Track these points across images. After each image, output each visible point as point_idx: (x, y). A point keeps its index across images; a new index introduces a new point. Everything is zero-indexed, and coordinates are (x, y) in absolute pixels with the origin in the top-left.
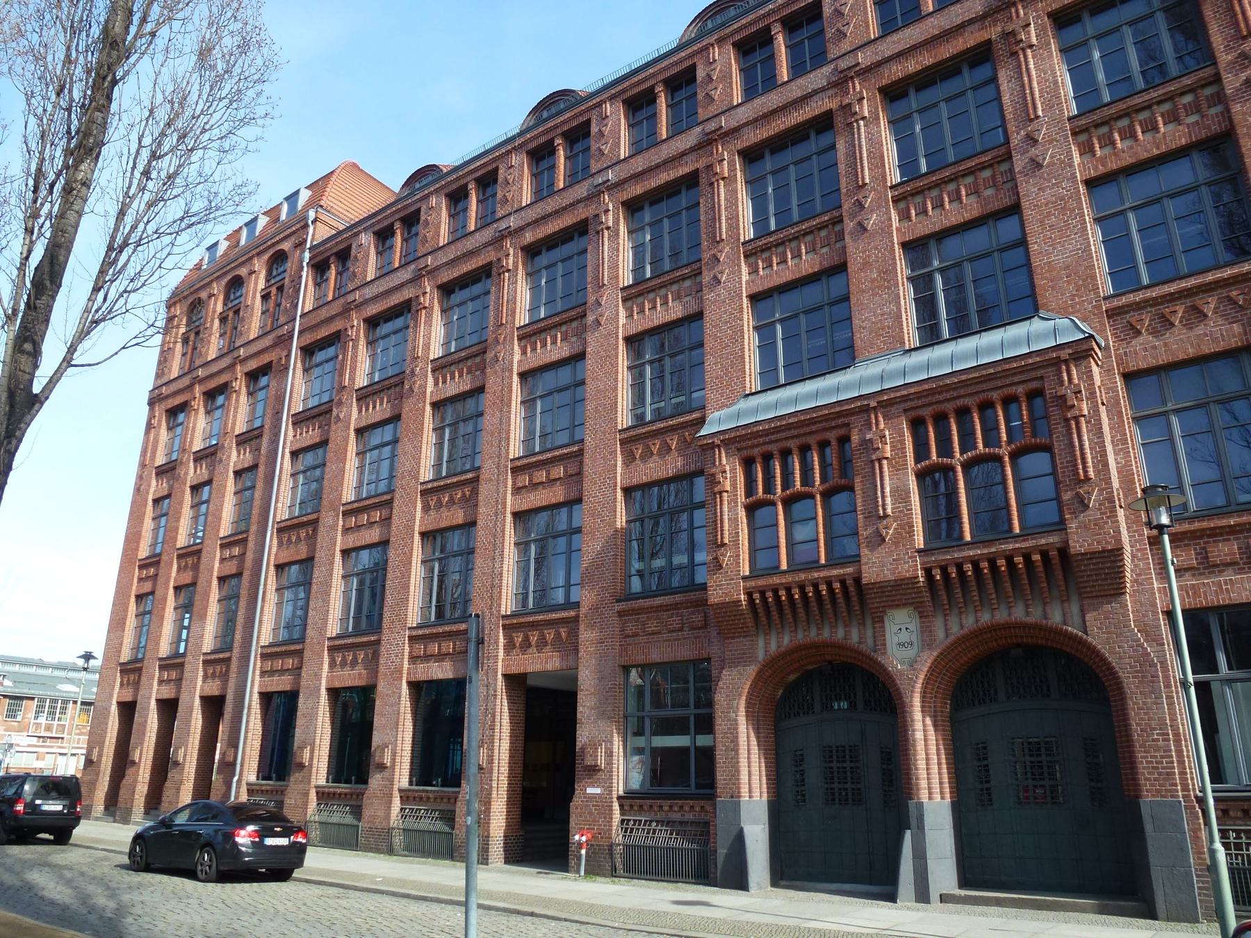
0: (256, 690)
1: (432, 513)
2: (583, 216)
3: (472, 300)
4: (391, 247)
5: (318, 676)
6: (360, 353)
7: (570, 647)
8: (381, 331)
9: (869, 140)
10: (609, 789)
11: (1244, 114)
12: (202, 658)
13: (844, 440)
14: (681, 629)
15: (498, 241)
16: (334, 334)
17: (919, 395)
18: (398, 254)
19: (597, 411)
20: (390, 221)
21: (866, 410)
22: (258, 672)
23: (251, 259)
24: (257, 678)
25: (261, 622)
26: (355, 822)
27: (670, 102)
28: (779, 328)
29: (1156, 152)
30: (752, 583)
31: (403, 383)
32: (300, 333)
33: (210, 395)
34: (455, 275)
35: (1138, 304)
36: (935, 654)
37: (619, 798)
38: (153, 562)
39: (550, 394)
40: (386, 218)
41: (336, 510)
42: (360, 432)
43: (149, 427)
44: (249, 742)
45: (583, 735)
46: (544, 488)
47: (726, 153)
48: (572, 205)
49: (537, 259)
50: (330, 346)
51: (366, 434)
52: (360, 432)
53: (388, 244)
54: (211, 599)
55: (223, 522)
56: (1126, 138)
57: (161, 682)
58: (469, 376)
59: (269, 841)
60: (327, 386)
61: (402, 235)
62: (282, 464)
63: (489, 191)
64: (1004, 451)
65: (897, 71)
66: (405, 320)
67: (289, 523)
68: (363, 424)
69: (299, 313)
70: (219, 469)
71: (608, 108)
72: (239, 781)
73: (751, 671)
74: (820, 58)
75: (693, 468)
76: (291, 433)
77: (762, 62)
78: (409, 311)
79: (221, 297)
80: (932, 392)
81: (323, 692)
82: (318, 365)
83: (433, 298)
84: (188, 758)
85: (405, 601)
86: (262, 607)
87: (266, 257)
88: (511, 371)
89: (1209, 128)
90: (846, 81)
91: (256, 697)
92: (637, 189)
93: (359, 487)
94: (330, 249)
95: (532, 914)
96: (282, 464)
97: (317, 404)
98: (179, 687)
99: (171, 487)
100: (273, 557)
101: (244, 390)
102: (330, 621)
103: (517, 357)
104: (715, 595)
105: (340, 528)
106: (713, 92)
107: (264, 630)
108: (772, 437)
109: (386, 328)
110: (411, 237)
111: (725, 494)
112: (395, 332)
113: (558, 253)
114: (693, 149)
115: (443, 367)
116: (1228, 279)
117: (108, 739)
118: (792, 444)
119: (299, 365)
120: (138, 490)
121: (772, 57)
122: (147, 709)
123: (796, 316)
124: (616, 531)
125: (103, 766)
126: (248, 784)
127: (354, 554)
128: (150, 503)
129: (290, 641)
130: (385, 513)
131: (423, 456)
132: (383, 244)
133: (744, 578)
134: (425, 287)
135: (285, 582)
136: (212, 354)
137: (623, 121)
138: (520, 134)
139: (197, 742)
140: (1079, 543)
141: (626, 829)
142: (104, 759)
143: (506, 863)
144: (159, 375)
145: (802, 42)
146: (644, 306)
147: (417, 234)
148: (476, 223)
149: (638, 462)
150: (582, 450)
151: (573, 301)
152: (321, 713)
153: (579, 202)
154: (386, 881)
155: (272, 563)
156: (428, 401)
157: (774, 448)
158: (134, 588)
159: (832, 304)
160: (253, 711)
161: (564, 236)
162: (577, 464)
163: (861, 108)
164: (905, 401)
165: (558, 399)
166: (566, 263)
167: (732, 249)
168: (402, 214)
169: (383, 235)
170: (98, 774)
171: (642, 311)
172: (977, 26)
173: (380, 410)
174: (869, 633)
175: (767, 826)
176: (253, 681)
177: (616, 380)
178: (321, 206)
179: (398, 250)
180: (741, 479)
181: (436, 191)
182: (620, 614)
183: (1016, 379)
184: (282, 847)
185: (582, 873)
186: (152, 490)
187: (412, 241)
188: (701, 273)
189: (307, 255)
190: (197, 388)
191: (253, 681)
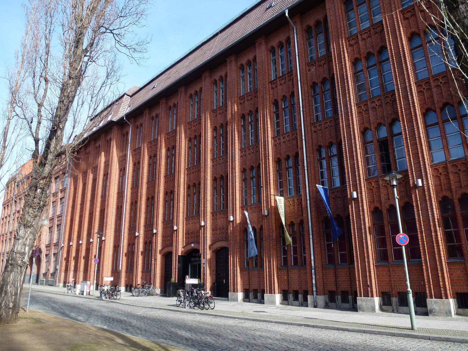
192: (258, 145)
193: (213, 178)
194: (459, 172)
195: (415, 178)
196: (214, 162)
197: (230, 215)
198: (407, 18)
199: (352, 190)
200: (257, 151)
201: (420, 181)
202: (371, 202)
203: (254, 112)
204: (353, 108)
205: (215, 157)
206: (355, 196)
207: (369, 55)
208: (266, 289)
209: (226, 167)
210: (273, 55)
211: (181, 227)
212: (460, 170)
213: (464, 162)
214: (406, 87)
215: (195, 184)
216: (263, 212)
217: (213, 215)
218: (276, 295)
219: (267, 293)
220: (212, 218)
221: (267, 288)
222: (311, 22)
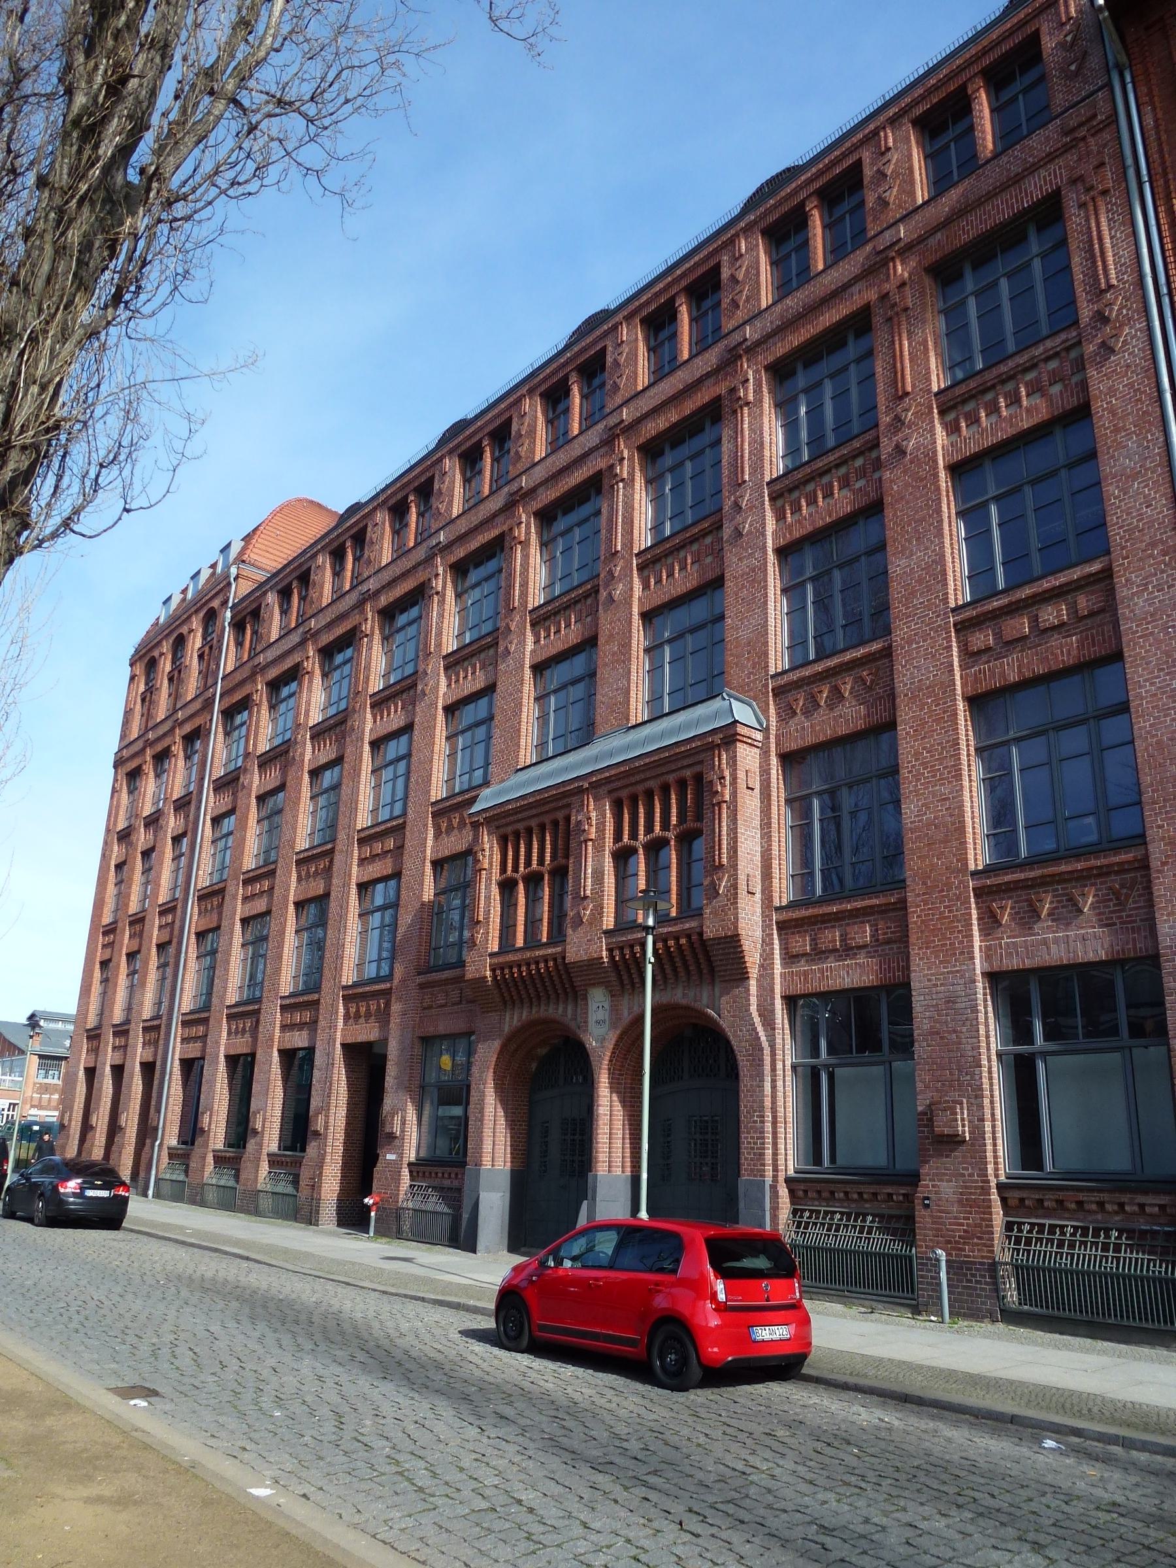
0: (177, 1057)
1: (303, 883)
2: (422, 580)
3: (579, 524)
5: (218, 1043)
6: (374, 653)
7: (384, 1018)
9: (625, 503)
10: (401, 1156)
11: (891, 481)
13: (568, 819)
14: (460, 1002)
15: (609, 442)
16: (591, 478)
17: (618, 777)
18: (295, 614)
19: (417, 783)
20: (286, 582)
21: (580, 791)
22: (179, 1039)
23: (190, 617)
24: (178, 1044)
25: (182, 989)
26: (897, 1248)
27: (827, 221)
28: (993, 509)
29: (828, 520)
30: (501, 959)
31: (597, 592)
32: (221, 696)
33: (274, 686)
34: (331, 639)
35: (795, 682)
36: (618, 1032)
37: (1000, 1187)
38: (110, 930)
39: (681, 636)
41: (237, 879)
43: (114, 791)
44: (170, 1108)
45: (389, 1102)
46: (369, 863)
47: (751, 372)
48: (414, 567)
49: (659, 461)
52: (450, 710)
53: (561, 407)
54: (151, 967)
55: (162, 889)
56: (952, 433)
57: (114, 1048)
59: (90, 1193)
60: (487, 612)
61: (492, 454)
62: (203, 831)
63: (596, 382)
64: (671, 835)
65: (652, 428)
67: (210, 889)
69: (221, 676)
70: (162, 834)
71: (320, 559)
72: (161, 1145)
73: (496, 1044)
74: (860, 237)
75: (1096, 651)
76: (212, 799)
77: (956, 139)
79: (170, 657)
80: (627, 774)
81: (222, 1059)
82: (473, 587)
83: (760, 386)
84: (129, 1122)
85: (278, 970)
86: (183, 975)
87: (201, 614)
88: (362, 740)
89: (1006, 431)
90: (736, 360)
91: (177, 1063)
92: (460, 553)
93: (450, 780)
94: (246, 608)
95: (216, 1250)
96: (203, 831)
97: (399, 678)
98: (255, 1038)
99: (235, 801)
100: (194, 925)
101: (318, 672)
102: (345, 968)
103: (369, 725)
104: (471, 972)
105: (240, 897)
106: (887, 194)
107: (185, 998)
108: (520, 816)
111: (590, 843)
112: (487, 579)
113: (685, 450)
114: (857, 279)
115: (546, 618)
116: (861, 658)
117: (76, 1104)
118: (533, 823)
119: (220, 729)
120: (103, 855)
121: (806, 244)
122: (103, 1075)
123: (1018, 489)
124: (423, 904)
125: (72, 1131)
126: (169, 1148)
128: (113, 868)
129: (378, 979)
131: (435, 770)
133: (492, 955)
134: (520, 517)
136: (274, 636)
137: (540, 415)
138: (567, 347)
139: (138, 1107)
140: (711, 930)
141: (800, 1223)
142: (73, 1123)
143: (339, 1225)
144: (123, 736)
145: (1014, 99)
146: (686, 560)
147: (508, 451)
148: (491, 486)
149: (799, 717)
150: (890, 646)
151: (708, 507)
152: (219, 1080)
153: (419, 564)
154: (197, 1233)
155: (193, 931)
157: (652, 784)
158: (99, 954)
159: (1070, 466)
160: (174, 1077)
161: (833, 339)
163: (903, 298)
164: (610, 782)
165: (690, 641)
167: (521, 617)
169: (399, 511)
170: (68, 1137)
171: (659, 581)
172: (712, 380)
174: (569, 1012)
175: (508, 1195)
176: (174, 1048)
177: (432, 751)
178: (243, 561)
179: (577, 410)
180: (497, 857)
182: (422, 986)
183: (685, 763)
184: (103, 1198)
185: (372, 1234)
186: (114, 856)
187: (503, 461)
188: (722, 526)
189: (228, 614)
190: (148, 751)
191: (174, 1048)
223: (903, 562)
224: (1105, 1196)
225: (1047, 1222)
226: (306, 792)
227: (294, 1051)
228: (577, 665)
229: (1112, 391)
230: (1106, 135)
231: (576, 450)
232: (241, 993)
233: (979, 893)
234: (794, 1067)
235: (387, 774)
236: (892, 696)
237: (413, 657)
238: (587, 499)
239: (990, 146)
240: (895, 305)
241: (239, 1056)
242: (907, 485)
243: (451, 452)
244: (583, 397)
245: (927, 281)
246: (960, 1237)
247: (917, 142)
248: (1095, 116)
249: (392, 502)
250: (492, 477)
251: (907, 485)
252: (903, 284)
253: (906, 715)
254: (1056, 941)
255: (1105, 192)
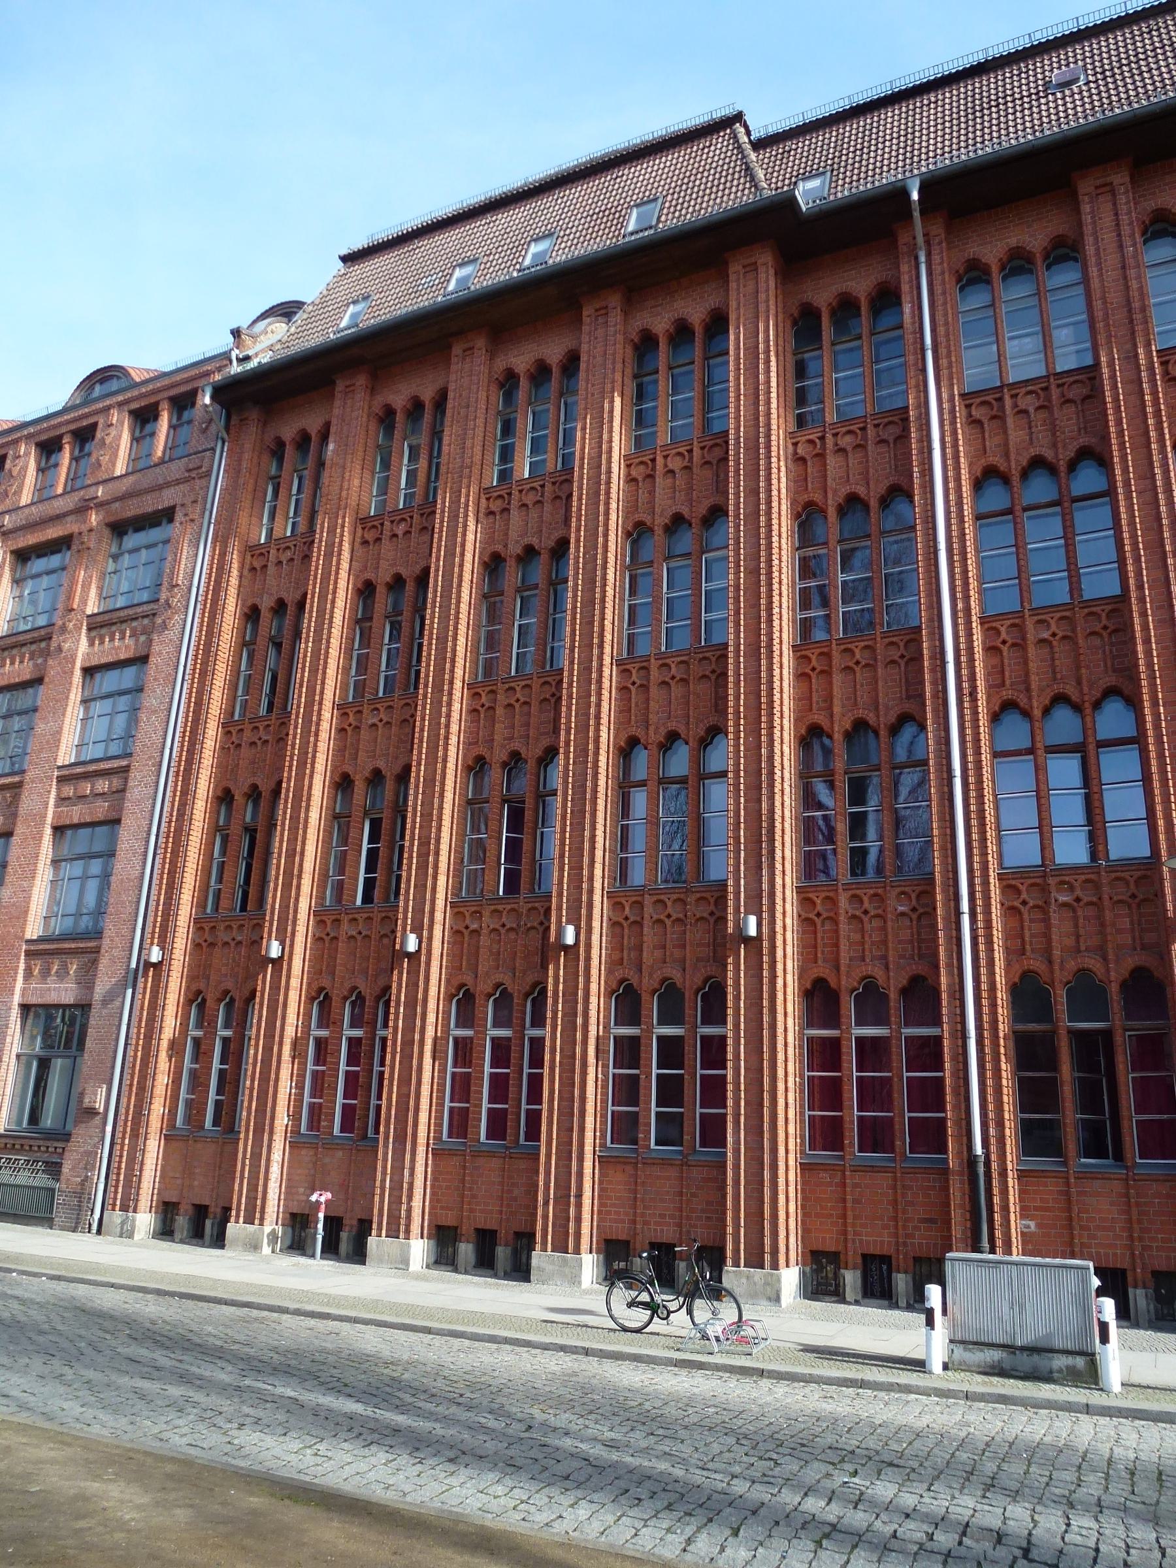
4: (153, 434)
8: (31, 569)
12: (24, 947)
26: (50, 1184)
40: (55, 427)
42: (89, 672)
50: (53, 553)
51: (98, 676)
52: (89, 672)
58: (31, 663)
61: (72, 453)
66: (63, 559)
68: (95, 662)
71: (115, 416)
78: (69, 548)
92: (31, 539)
109: (38, 565)
110: (83, 457)
112: (49, 573)
127: (69, 833)
130: (116, 782)
132: (48, 459)
135: (65, 852)
147: (89, 454)
156: (78, 665)
162: (122, 778)
163: (89, 540)
166: (134, 555)
168: (73, 427)
173: (122, 646)
181: (120, 405)
187: (83, 462)
192: (286, 720)
193: (220, 794)
194: (863, 916)
195: (742, 910)
196: (229, 732)
197: (152, 944)
198: (491, 513)
199: (564, 919)
200: (281, 739)
201: (752, 920)
202: (614, 964)
203: (291, 610)
204: (606, 672)
205: (236, 717)
206: (570, 939)
207: (678, 522)
208: (375, 1219)
209: (409, 743)
210: (385, 435)
211: (178, 954)
212: (866, 912)
213: (1038, 881)
214: (589, 669)
215: (254, 787)
216: (398, 940)
217: (320, 923)
218: (138, 1216)
219: (237, 1222)
220: (193, 940)
221: (736, 1238)
222: (288, 431)
223: (43, 726)
224: (41, 1143)
225: (14, 1157)
226: (75, 695)
227: (49, 1009)
228: (127, 677)
229: (160, 653)
230: (204, 481)
231: (61, 505)
232: (47, 925)
233: (28, 954)
234: (18, 1056)
235: (98, 707)
236: (15, 815)
237: (48, 607)
238: (158, 524)
239: (159, 454)
240: (82, 543)
241: (57, 1006)
242: (58, 673)
243: (120, 405)
244: (171, 426)
245: (107, 532)
246: (1159, 1249)
247: (130, 427)
248: (201, 467)
249: (44, 437)
250: (68, 474)
251: (58, 673)
252: (91, 530)
253: (19, 830)
254: (55, 989)
255: (192, 520)
